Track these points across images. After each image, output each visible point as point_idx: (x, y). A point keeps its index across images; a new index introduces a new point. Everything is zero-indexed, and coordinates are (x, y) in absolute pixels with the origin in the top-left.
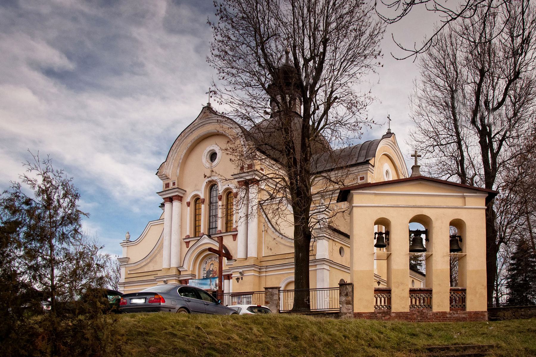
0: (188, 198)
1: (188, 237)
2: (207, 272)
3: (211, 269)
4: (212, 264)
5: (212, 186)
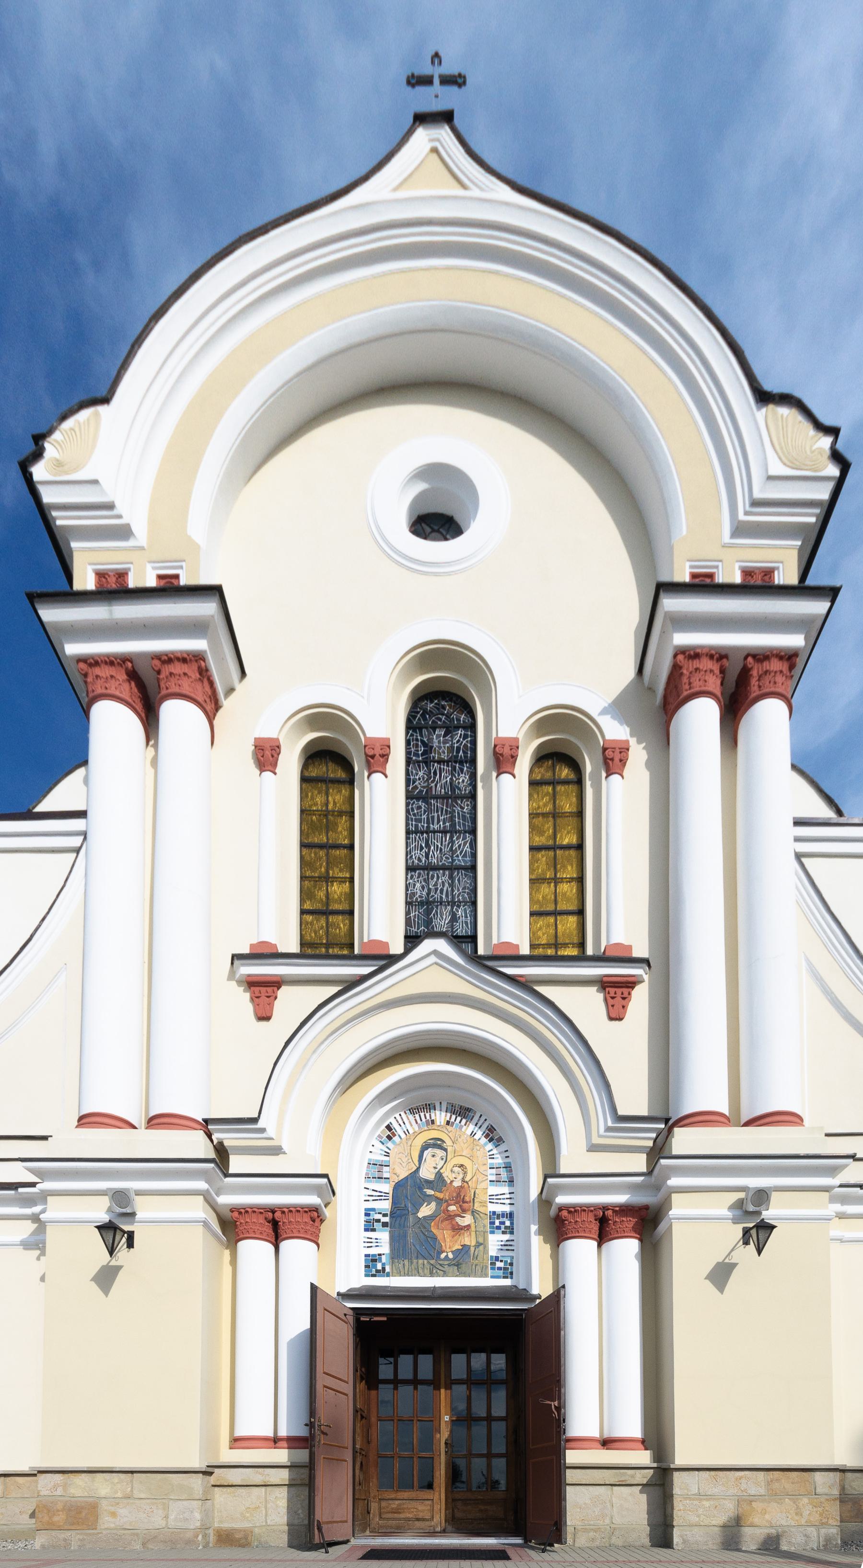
0: (269, 703)
1: (263, 953)
2: (399, 1187)
3: (427, 1173)
4: (437, 1144)
5: (444, 701)
